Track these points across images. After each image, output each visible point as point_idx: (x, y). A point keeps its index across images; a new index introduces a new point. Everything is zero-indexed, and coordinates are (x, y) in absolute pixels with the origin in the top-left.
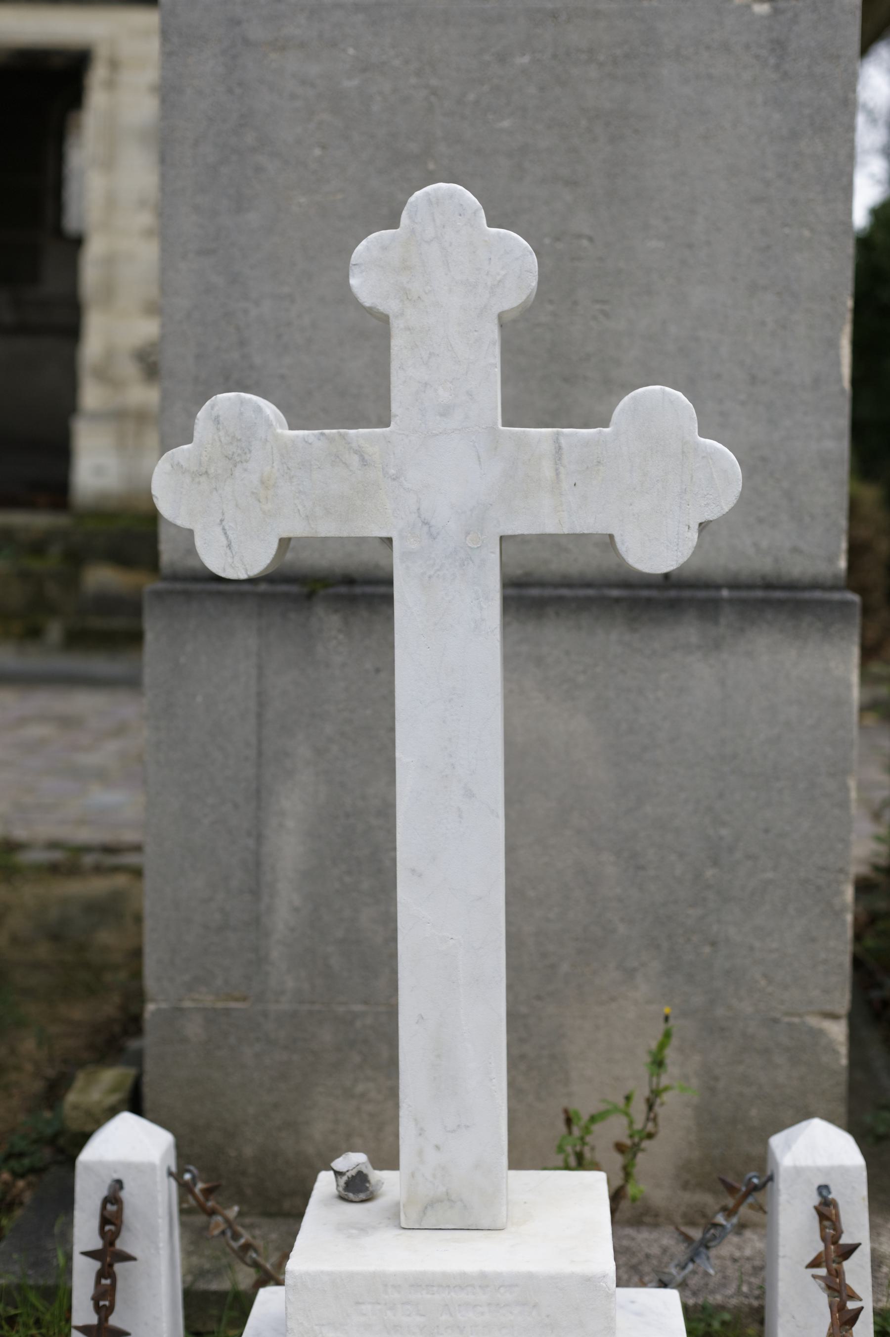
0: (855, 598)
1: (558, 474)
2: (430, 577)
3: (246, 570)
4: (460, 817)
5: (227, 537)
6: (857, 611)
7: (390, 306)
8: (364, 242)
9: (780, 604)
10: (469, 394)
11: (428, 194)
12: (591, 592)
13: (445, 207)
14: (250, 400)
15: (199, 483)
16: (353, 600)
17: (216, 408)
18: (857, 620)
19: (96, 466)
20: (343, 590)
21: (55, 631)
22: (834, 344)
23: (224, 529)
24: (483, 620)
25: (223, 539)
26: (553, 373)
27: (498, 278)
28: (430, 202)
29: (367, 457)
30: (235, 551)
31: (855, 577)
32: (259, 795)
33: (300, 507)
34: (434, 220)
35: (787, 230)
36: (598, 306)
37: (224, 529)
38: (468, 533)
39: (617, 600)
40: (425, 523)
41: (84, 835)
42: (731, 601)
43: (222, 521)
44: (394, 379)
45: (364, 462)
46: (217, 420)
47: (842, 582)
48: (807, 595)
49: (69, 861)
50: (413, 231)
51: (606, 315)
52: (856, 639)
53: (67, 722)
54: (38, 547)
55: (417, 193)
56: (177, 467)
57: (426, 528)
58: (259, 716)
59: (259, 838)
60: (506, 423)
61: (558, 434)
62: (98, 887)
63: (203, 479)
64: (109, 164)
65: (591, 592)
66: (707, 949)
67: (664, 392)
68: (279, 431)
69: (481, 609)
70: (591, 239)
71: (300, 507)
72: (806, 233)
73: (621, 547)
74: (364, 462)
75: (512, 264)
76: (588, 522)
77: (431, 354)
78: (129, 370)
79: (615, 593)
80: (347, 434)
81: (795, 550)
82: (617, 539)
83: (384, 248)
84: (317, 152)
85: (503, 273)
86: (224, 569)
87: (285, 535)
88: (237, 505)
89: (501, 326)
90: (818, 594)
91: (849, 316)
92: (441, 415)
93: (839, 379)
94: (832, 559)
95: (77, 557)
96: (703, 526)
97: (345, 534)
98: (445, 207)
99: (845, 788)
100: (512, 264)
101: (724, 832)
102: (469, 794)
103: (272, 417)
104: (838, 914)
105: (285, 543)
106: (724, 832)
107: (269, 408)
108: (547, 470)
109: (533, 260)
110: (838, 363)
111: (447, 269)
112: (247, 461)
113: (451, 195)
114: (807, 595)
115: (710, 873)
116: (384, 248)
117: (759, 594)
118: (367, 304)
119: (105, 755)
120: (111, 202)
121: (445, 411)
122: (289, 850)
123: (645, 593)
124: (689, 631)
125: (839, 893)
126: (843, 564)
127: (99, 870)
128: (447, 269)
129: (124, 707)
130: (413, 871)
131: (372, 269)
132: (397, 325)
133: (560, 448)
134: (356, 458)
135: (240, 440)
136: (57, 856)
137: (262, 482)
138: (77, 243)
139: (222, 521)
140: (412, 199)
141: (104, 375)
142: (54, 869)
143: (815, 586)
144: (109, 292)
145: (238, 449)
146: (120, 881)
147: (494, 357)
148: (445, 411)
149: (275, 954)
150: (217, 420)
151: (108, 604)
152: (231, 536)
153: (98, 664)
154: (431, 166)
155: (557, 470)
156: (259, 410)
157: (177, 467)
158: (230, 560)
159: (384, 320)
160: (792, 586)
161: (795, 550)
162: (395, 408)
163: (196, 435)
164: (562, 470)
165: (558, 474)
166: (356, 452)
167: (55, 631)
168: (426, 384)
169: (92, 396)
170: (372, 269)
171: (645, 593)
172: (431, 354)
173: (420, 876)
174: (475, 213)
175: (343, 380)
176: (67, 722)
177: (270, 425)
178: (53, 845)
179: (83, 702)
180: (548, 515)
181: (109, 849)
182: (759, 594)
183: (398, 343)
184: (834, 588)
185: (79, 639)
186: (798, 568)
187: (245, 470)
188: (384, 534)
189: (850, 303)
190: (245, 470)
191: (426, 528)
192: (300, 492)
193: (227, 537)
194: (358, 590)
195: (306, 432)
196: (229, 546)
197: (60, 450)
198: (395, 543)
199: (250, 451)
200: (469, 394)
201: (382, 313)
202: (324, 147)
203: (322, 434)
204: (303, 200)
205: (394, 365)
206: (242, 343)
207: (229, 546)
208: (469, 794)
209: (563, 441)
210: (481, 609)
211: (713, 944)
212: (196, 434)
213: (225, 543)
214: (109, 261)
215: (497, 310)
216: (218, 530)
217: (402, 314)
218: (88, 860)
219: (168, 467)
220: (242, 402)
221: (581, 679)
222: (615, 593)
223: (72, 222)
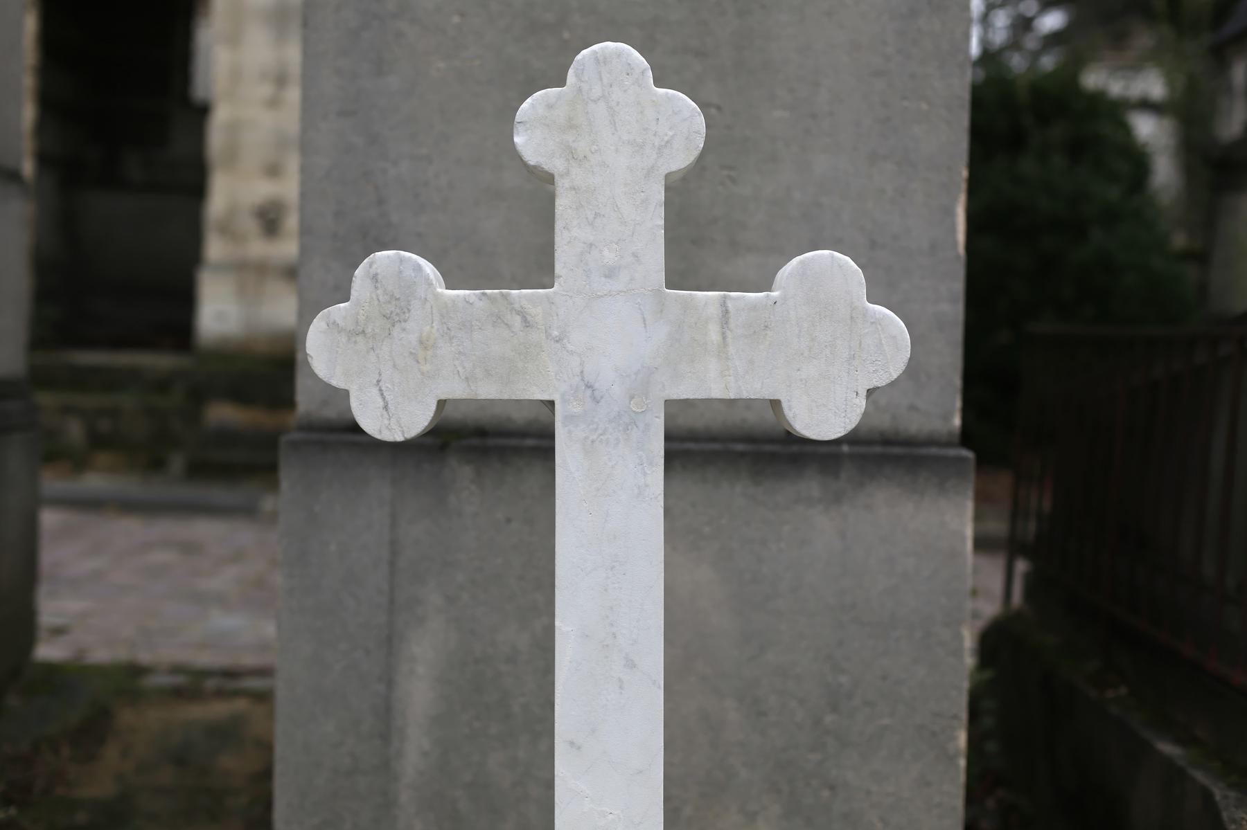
0: (969, 454)
1: (724, 338)
2: (593, 442)
3: (403, 432)
4: (621, 687)
5: (384, 399)
6: (971, 467)
7: (554, 164)
8: (529, 100)
9: (897, 460)
10: (635, 255)
11: (595, 52)
12: (716, 446)
13: (612, 67)
14: (410, 258)
15: (355, 342)
16: (485, 452)
17: (375, 266)
18: (972, 476)
19: (219, 312)
20: (475, 441)
21: (177, 462)
22: (950, 213)
23: (380, 390)
24: (647, 486)
25: (380, 400)
26: (710, 237)
27: (666, 138)
28: (597, 60)
29: (529, 318)
30: (392, 410)
31: (967, 437)
32: (391, 642)
33: (460, 369)
34: (601, 79)
35: (906, 103)
36: (725, 172)
37: (380, 390)
38: (632, 398)
39: (742, 455)
40: (589, 386)
41: (205, 659)
42: (851, 456)
43: (378, 381)
44: (557, 239)
45: (527, 324)
46: (375, 278)
47: (956, 439)
48: (924, 451)
49: (193, 684)
50: (580, 90)
51: (733, 180)
52: (970, 493)
53: (189, 548)
54: (162, 384)
55: (584, 52)
56: (332, 325)
57: (589, 392)
58: (392, 564)
59: (390, 683)
60: (670, 285)
61: (725, 297)
62: (218, 710)
63: (360, 339)
64: (234, 39)
65: (716, 446)
66: (826, 793)
67: (833, 257)
68: (439, 290)
69: (645, 474)
70: (719, 108)
71: (460, 369)
72: (924, 106)
73: (789, 414)
74: (527, 324)
75: (676, 124)
76: (754, 387)
77: (597, 215)
78: (250, 225)
79: (740, 447)
80: (509, 294)
81: (912, 408)
82: (785, 405)
83: (550, 107)
84: (456, 19)
85: (671, 133)
86: (380, 432)
87: (443, 397)
88: (394, 366)
89: (667, 189)
90: (934, 451)
91: (964, 186)
92: (606, 277)
93: (955, 243)
94: (947, 417)
95: (199, 394)
96: (870, 392)
97: (506, 397)
98: (612, 67)
99: (958, 637)
100: (676, 124)
101: (843, 679)
102: (631, 664)
103: (432, 276)
104: (952, 759)
105: (441, 404)
106: (843, 679)
107: (428, 268)
108: (714, 334)
109: (700, 121)
110: (953, 230)
111: (613, 129)
112: (405, 321)
113: (619, 54)
114: (924, 451)
115: (829, 719)
116: (550, 107)
117: (878, 449)
118: (532, 163)
119: (224, 580)
120: (236, 74)
121: (610, 273)
122: (419, 694)
123: (769, 448)
124: (812, 485)
125: (954, 739)
126: (957, 421)
127: (220, 694)
128: (613, 129)
129: (243, 534)
130: (572, 743)
131: (536, 128)
132: (562, 185)
133: (727, 312)
134: (518, 318)
135: (397, 299)
136: (179, 680)
137: (421, 342)
138: (202, 112)
139: (378, 381)
140: (579, 57)
141: (227, 230)
142: (178, 694)
143: (931, 441)
144: (232, 155)
145: (395, 310)
146: (240, 705)
147: (657, 219)
148: (610, 273)
149: (405, 797)
150: (375, 278)
151: (227, 437)
152: (388, 398)
153: (217, 493)
154: (566, 35)
155: (723, 333)
156: (419, 268)
157: (332, 325)
158: (386, 422)
159: (549, 179)
160: (909, 442)
161: (912, 408)
162: (559, 268)
163: (354, 294)
164: (729, 334)
165: (724, 338)
166: (518, 313)
167: (177, 462)
168: (591, 245)
169: (215, 248)
170: (536, 128)
171: (769, 448)
172: (597, 215)
173: (579, 748)
174: (643, 73)
175: (508, 238)
176: (189, 548)
177: (430, 284)
178: (176, 669)
179: (205, 530)
180: (723, 378)
181: (230, 674)
182: (878, 449)
183: (563, 204)
184: (948, 444)
185: (200, 470)
186: (915, 425)
187: (404, 330)
188: (546, 397)
189: (965, 173)
190: (404, 330)
191: (589, 392)
192: (460, 353)
193: (384, 399)
194: (491, 442)
195: (467, 292)
196: (386, 407)
197: (183, 298)
198: (557, 406)
199: (409, 310)
200: (635, 255)
201: (547, 172)
202: (462, 15)
203: (484, 294)
204: (441, 65)
205: (559, 225)
206: (381, 202)
207: (386, 407)
208: (631, 664)
209: (730, 304)
210: (645, 474)
211: (832, 788)
212: (353, 292)
213: (382, 404)
214: (234, 128)
215: (664, 170)
216: (375, 391)
217: (568, 173)
218: (211, 684)
219: (323, 325)
220: (402, 260)
221: (707, 530)
222: (740, 447)
223: (199, 91)
